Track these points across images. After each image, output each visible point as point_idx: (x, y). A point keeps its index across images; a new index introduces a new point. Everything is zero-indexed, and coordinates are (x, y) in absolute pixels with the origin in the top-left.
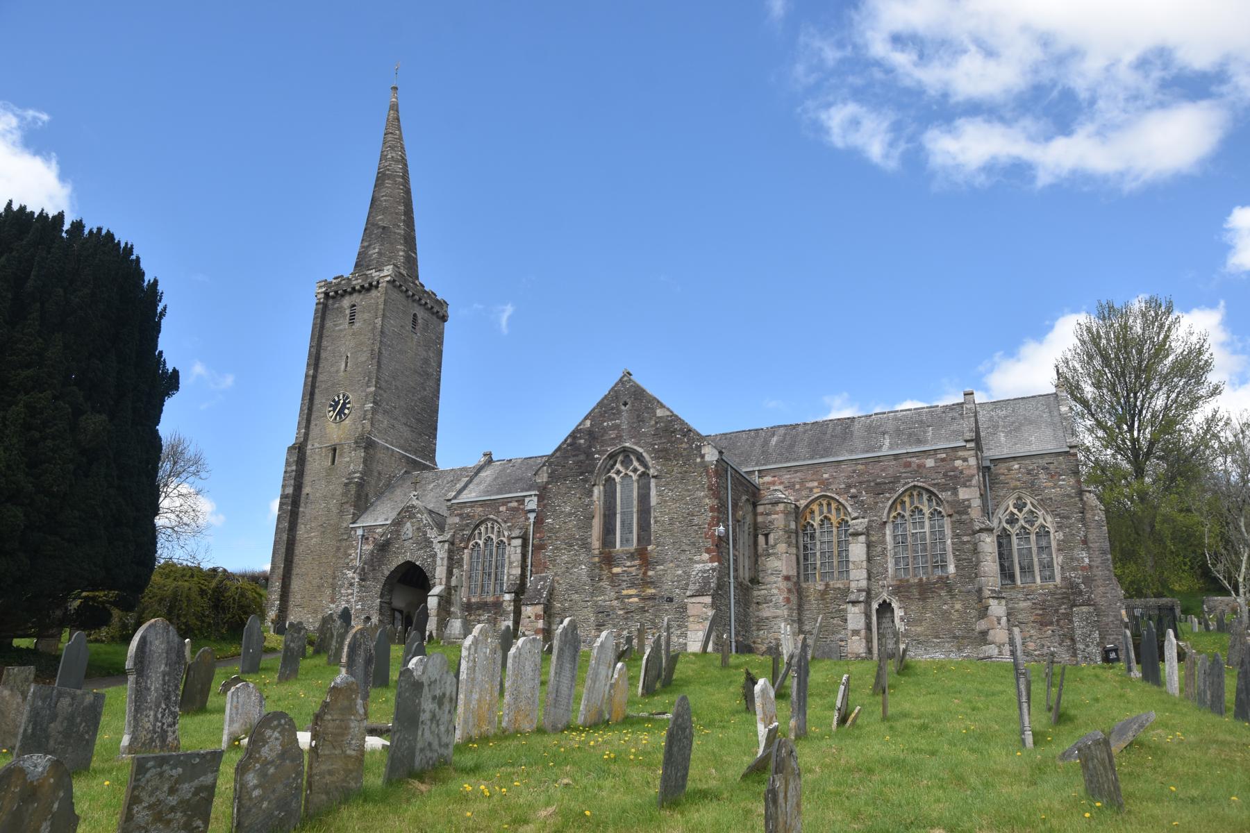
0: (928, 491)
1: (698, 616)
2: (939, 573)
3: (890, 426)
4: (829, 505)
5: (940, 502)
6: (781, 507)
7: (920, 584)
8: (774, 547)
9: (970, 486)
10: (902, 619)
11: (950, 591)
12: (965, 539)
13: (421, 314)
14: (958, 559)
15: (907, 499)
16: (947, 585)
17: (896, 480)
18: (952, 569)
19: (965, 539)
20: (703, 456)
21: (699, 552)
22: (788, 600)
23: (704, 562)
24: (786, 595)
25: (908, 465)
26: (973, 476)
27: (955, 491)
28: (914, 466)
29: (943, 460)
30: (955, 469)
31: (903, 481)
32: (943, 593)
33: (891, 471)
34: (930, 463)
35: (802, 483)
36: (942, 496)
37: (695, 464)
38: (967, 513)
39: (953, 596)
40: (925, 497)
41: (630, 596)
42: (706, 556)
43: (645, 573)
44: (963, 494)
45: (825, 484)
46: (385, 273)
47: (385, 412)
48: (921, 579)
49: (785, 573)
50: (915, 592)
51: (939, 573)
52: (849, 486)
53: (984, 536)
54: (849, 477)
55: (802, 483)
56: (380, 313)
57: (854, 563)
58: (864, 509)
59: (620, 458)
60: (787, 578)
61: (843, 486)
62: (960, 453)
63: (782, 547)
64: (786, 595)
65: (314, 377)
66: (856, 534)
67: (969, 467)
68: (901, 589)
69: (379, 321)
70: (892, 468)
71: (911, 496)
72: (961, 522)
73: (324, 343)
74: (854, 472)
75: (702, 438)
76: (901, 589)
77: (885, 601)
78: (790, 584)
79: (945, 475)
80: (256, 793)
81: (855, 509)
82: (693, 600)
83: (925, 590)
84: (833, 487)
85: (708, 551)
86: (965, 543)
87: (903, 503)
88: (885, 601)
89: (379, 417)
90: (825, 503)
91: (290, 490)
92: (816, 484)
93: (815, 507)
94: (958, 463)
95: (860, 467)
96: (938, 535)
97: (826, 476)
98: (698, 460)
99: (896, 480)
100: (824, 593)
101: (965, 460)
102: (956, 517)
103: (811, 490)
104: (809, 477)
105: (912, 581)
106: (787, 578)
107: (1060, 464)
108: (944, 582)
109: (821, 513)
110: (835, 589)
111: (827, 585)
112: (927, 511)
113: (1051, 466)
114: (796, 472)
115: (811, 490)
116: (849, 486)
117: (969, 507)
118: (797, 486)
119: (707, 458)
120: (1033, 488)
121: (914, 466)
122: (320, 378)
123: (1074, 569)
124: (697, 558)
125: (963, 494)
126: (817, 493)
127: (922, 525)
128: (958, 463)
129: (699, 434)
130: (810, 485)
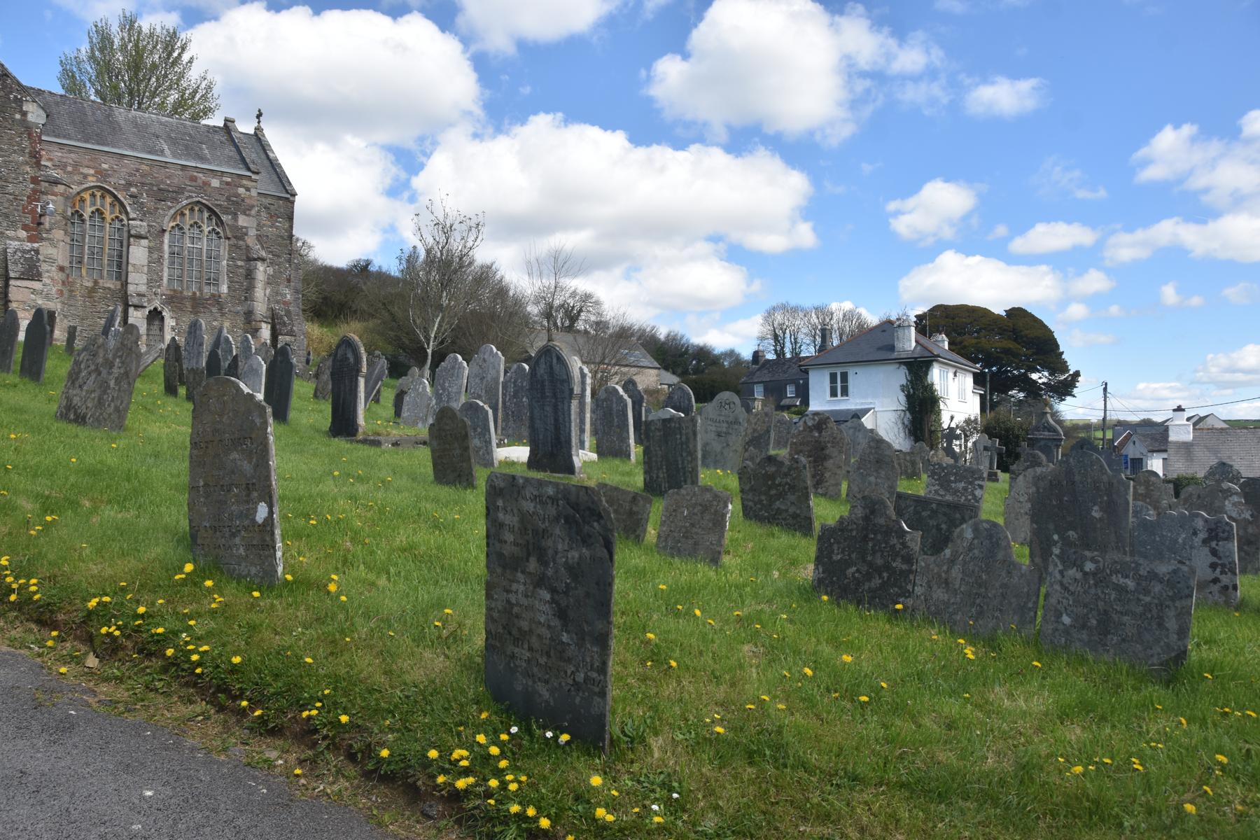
0: (210, 209)
1: (24, 302)
2: (213, 290)
3: (948, 233)
4: (103, 197)
5: (220, 222)
6: (61, 188)
7: (193, 298)
8: (48, 231)
10: (173, 329)
11: (221, 309)
12: (239, 263)
14: (231, 281)
15: (187, 212)
16: (219, 303)
17: (180, 191)
18: (224, 289)
19: (239, 263)
20: (24, 114)
21: (13, 225)
22: (61, 292)
23: (18, 239)
25: (193, 179)
26: (253, 206)
27: (235, 218)
28: (200, 182)
29: (228, 184)
30: (238, 195)
31: (187, 194)
32: (214, 310)
33: (176, 181)
34: (215, 183)
35: (76, 165)
36: (224, 218)
37: (14, 120)
38: (243, 240)
39: (223, 315)
40: (206, 215)
42: (23, 234)
44: (242, 221)
45: (102, 174)
48: (194, 293)
50: (188, 304)
51: (213, 290)
52: (129, 184)
53: (259, 264)
54: (131, 175)
55: (76, 165)
57: (134, 265)
58: (145, 213)
60: (62, 269)
62: (245, 182)
63: (58, 234)
66: (140, 237)
67: (250, 197)
68: (174, 300)
70: (178, 178)
71: (192, 210)
72: (238, 247)
74: (137, 170)
75: (25, 90)
76: (174, 300)
77: (155, 309)
79: (228, 199)
80: (318, 704)
81: (134, 210)
82: (19, 283)
83: (198, 304)
84: (112, 180)
85: (25, 228)
86: (238, 267)
87: (183, 214)
88: (155, 309)
90: (98, 194)
92: (92, 171)
93: (87, 196)
94: (241, 190)
95: (144, 167)
96: (213, 257)
97: (105, 166)
98: (18, 116)
99: (180, 191)
100: (91, 291)
101: (248, 189)
102: (233, 241)
104: (86, 163)
105: (185, 293)
106: (62, 269)
108: (216, 299)
109: (93, 204)
110: (105, 288)
111: (96, 282)
112: (206, 229)
114: (70, 152)
115: (85, 176)
116: (129, 184)
117: (246, 234)
118: (69, 169)
119: (30, 118)
121: (200, 182)
123: (278, 302)
124: (10, 233)
125: (242, 221)
126: (92, 181)
127: (102, 228)
129: (19, 84)
130: (85, 171)
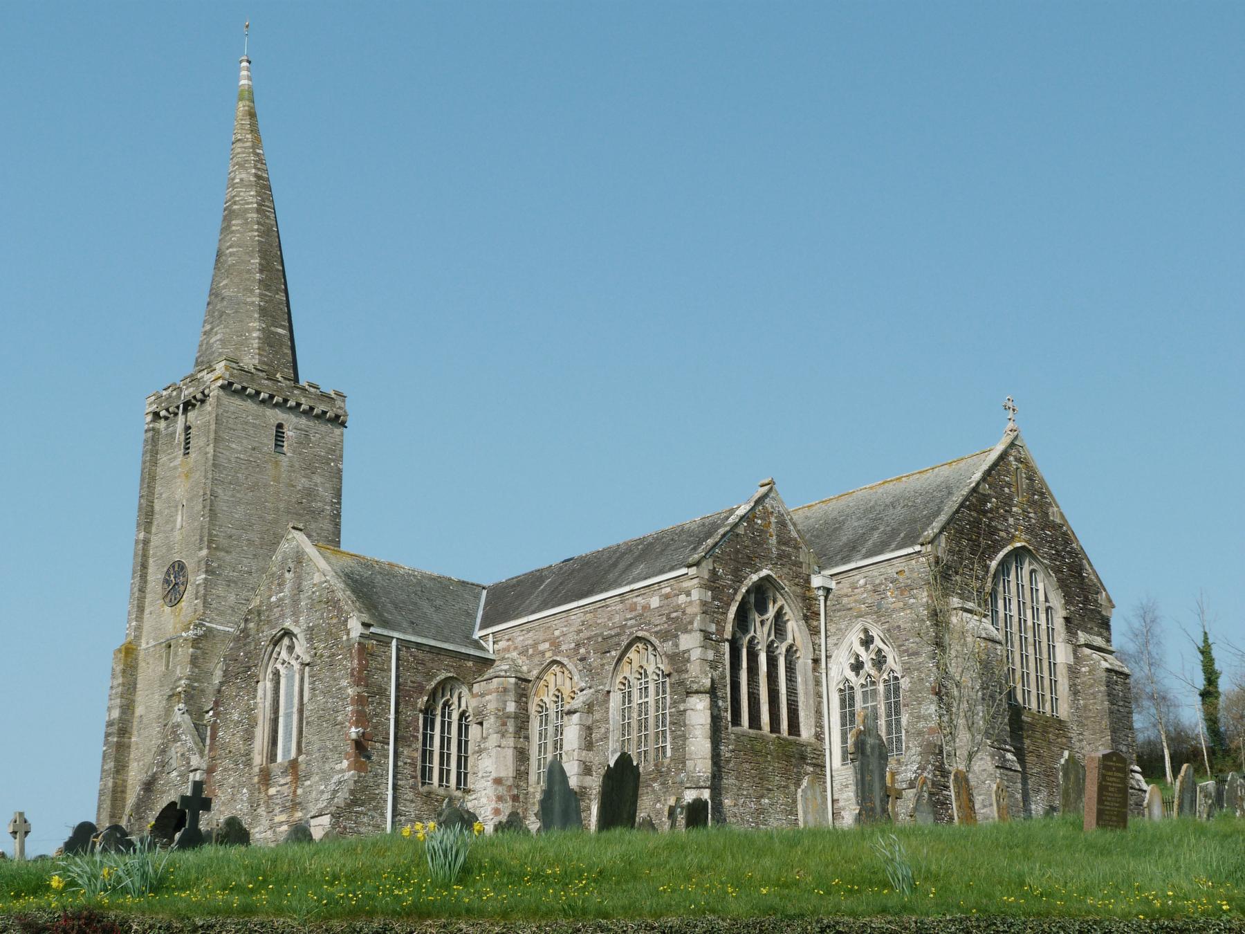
9: (690, 631)
13: (292, 423)
24: (493, 805)
29: (667, 596)
33: (617, 619)
41: (281, 823)
43: (295, 792)
45: (555, 645)
46: (218, 373)
47: (229, 582)
49: (494, 775)
52: (578, 645)
55: (535, 646)
56: (212, 436)
59: (286, 641)
61: (573, 645)
64: (493, 805)
65: (146, 542)
69: (210, 449)
73: (158, 489)
78: (501, 790)
89: (220, 590)
91: (116, 714)
92: (547, 645)
101: (688, 594)
103: (543, 653)
106: (498, 781)
107: (912, 570)
113: (901, 578)
114: (529, 631)
115: (543, 653)
117: (688, 660)
118: (531, 651)
120: (878, 612)
122: (155, 541)
128: (682, 599)
